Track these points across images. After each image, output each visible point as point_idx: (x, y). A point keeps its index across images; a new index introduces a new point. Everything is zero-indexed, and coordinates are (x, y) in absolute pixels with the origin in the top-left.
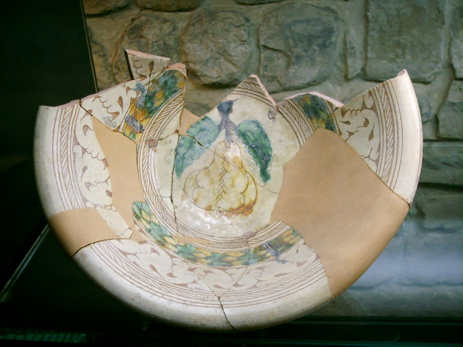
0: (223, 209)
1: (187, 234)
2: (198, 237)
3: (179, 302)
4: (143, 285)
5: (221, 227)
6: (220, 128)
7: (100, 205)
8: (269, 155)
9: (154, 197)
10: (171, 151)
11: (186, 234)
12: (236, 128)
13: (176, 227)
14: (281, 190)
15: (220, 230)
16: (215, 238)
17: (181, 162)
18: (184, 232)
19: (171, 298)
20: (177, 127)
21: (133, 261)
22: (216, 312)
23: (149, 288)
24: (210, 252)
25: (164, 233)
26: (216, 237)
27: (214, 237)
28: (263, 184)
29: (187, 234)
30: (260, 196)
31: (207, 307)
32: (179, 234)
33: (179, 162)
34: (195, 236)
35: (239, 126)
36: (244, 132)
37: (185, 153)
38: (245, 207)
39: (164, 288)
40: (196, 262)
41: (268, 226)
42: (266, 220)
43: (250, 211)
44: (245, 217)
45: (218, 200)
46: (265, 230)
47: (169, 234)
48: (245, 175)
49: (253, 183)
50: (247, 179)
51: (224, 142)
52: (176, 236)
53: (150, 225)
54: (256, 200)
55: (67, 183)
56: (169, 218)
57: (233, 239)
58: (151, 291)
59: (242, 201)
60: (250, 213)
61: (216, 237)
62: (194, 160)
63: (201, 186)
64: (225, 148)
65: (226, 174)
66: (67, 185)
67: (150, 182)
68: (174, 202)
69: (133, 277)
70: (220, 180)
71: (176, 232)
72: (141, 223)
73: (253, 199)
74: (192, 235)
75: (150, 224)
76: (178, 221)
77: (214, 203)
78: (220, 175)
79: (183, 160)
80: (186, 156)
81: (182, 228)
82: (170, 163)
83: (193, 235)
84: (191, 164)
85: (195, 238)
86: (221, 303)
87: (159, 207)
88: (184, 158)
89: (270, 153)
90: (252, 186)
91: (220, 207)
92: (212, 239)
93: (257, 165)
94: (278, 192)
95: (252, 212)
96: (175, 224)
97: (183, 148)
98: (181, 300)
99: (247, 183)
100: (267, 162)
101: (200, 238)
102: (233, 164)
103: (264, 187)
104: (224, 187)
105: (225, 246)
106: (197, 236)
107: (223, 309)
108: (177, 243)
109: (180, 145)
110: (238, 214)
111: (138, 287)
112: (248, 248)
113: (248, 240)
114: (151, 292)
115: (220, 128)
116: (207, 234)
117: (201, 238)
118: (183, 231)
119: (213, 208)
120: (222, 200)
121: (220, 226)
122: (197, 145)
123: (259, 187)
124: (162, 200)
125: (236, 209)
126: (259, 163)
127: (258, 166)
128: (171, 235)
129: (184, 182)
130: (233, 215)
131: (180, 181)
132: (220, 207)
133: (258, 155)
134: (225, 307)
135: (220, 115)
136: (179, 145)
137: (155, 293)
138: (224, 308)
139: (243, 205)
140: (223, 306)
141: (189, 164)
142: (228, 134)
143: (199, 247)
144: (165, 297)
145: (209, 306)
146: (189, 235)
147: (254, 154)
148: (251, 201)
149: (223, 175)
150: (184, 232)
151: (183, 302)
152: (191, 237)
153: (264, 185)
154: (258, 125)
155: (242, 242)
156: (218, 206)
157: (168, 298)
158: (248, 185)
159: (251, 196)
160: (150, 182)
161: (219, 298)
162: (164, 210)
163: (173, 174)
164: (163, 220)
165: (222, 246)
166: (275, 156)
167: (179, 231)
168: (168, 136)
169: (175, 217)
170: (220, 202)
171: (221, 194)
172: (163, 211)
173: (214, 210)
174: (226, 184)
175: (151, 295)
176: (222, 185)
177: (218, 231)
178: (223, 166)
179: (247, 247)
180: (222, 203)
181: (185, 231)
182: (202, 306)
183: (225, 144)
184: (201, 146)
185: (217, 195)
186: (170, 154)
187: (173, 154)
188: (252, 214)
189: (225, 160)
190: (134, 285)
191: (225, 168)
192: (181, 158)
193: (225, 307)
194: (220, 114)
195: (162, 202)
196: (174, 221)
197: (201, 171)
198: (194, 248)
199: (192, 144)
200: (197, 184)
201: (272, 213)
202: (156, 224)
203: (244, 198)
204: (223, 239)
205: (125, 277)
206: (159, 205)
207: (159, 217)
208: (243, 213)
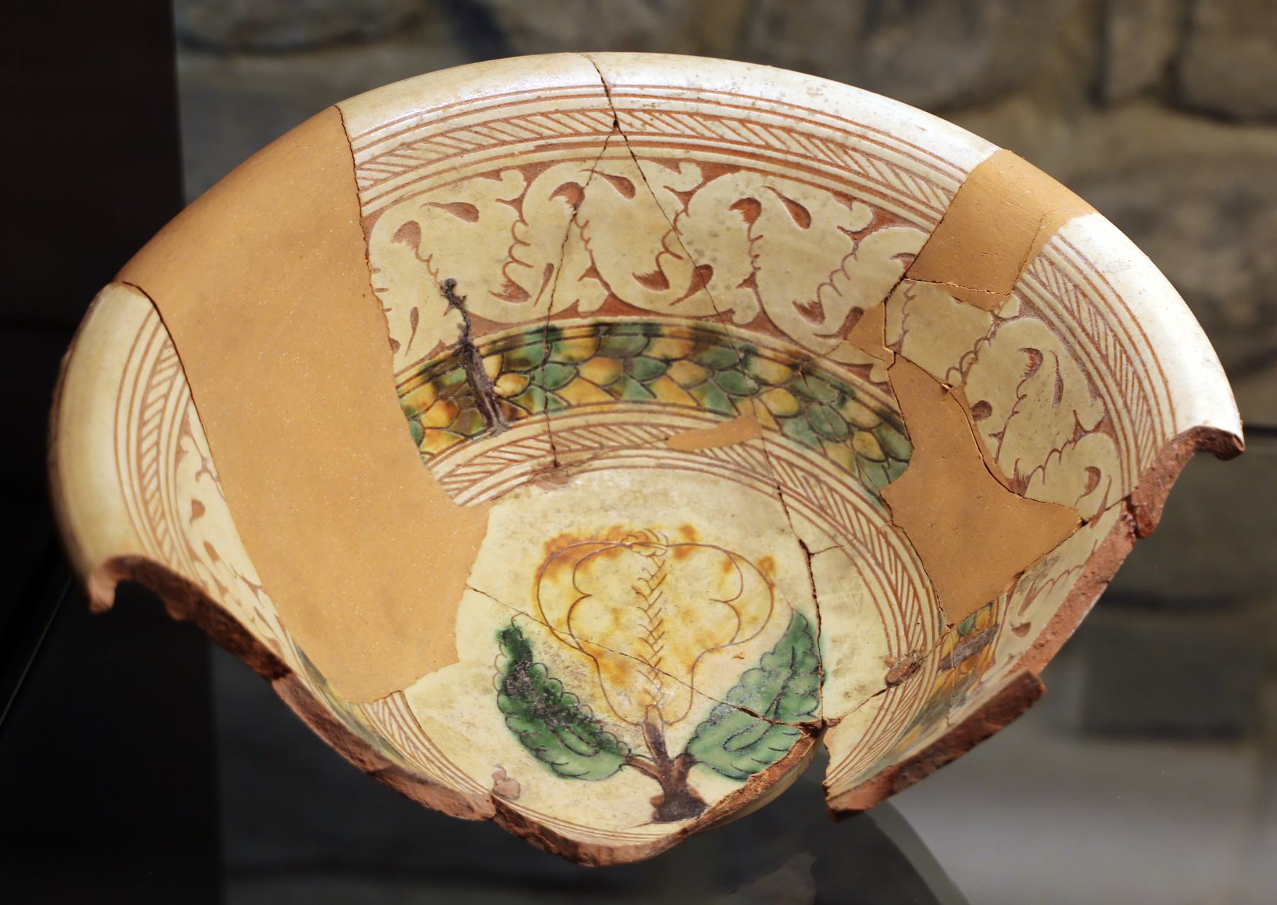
0: (639, 552)
1: (735, 457)
2: (703, 454)
3: (712, 92)
4: (810, 122)
5: (636, 498)
6: (688, 759)
7: (988, 339)
8: (508, 695)
9: (859, 535)
10: (836, 672)
11: (739, 455)
12: (631, 760)
13: (772, 466)
14: (461, 597)
15: (640, 491)
16: (653, 462)
17: (799, 652)
18: (745, 460)
19: (735, 101)
20: (834, 735)
21: (855, 204)
22: (619, 74)
23: (791, 117)
24: (660, 399)
25: (802, 423)
26: (648, 467)
27: (654, 467)
28: (520, 621)
29: (735, 457)
30: (527, 588)
31: (642, 87)
32: (758, 443)
33: (805, 653)
34: (711, 458)
35: (620, 766)
36: (602, 752)
37: (791, 677)
38: (571, 561)
39: (756, 134)
40: (695, 328)
41: (495, 498)
42: (499, 514)
43: (554, 549)
44: (566, 531)
45: (660, 576)
46: (505, 486)
47: (789, 427)
48: (579, 641)
49: (551, 624)
50: (574, 632)
51: (667, 723)
52: (767, 434)
53: (848, 420)
54: (539, 577)
55: (1083, 304)
56: (800, 490)
57: (596, 463)
58: (785, 110)
59: (579, 576)
60: (554, 541)
61: (648, 467)
62: (759, 667)
63: (720, 605)
64: (660, 706)
65: (644, 634)
66: (1081, 297)
67: (881, 566)
68: (795, 545)
69: (838, 136)
70: (661, 622)
71: (769, 447)
72: (872, 403)
73: (545, 582)
74: (723, 456)
75: (848, 424)
76: (770, 490)
77: (671, 566)
78: (663, 633)
79: (793, 658)
80: (785, 673)
81: (754, 470)
82: (834, 641)
83: (717, 458)
84: (765, 654)
85: (711, 450)
86: (610, 100)
87: (835, 510)
88: (793, 665)
89: (503, 699)
90: (556, 614)
91: (648, 556)
92: (658, 458)
93: (546, 669)
94: (469, 593)
95: (548, 545)
96: (777, 477)
97: (801, 691)
98: (708, 102)
99: (572, 623)
100: (512, 674)
101: (697, 451)
102: (628, 658)
103: (514, 613)
104: (645, 605)
105: (619, 435)
106: (706, 456)
107: (603, 81)
108: (756, 401)
109: (813, 696)
110: (592, 541)
111: (821, 113)
112: (548, 420)
113: (550, 459)
114: (786, 107)
115: (688, 759)
116: (677, 471)
117: (692, 453)
118: (750, 459)
119: (671, 552)
120: (646, 576)
121: (641, 501)
122: (759, 708)
123: (530, 609)
124: (833, 538)
125: (594, 555)
126: (541, 674)
127: (540, 668)
128: (781, 426)
129: (776, 605)
130: (604, 538)
131: (789, 604)
132: (648, 556)
133: (545, 695)
134: (598, 86)
135: (693, 790)
136: (813, 693)
137: (775, 105)
138: (601, 83)
139: (577, 566)
140: (602, 90)
141: (773, 654)
142: (658, 745)
143: (694, 413)
144: (749, 102)
145: (637, 91)
146: (730, 452)
147: (559, 694)
148: (554, 576)
149: (654, 634)
150: (745, 460)
151: (703, 95)
152: (721, 449)
153: (516, 618)
154: (554, 768)
155: (571, 451)
156: (655, 558)
157: (741, 101)
158: (569, 618)
159: (558, 589)
160: (881, 566)
161: (616, 124)
162: (821, 507)
163: (819, 617)
164: (816, 471)
165: (627, 435)
166: (486, 691)
167: (760, 457)
168: (859, 707)
169: (783, 501)
170: (653, 570)
171: (652, 590)
172: (823, 502)
173: (668, 546)
174: (641, 613)
175: (784, 100)
176: (652, 612)
177: (644, 486)
178: (656, 653)
179: (554, 425)
180: (643, 569)
181: (743, 464)
182: (654, 87)
183: (661, 716)
184: (741, 705)
185: (662, 588)
186: (839, 662)
187: (829, 664)
188: (547, 539)
189: (653, 668)
190: (831, 113)
191: (650, 649)
192: (802, 663)
193: (598, 86)
194: (696, 792)
195: (832, 532)
196: (781, 487)
197: (727, 642)
198: (707, 404)
199: (774, 707)
200: (733, 608)
201: (485, 534)
202: (830, 440)
203: (577, 584)
204: (628, 461)
205: (859, 128)
206: (838, 518)
207: (829, 474)
208: (575, 544)
